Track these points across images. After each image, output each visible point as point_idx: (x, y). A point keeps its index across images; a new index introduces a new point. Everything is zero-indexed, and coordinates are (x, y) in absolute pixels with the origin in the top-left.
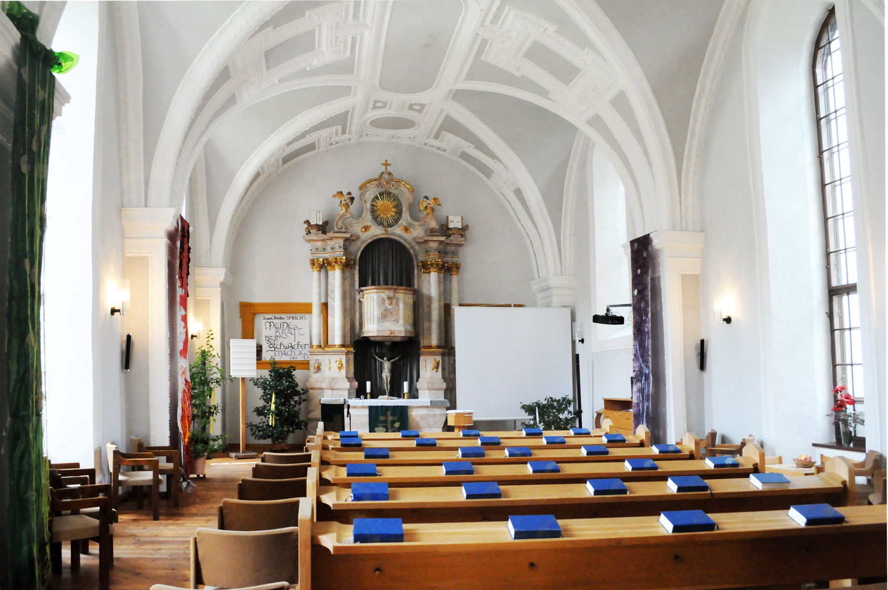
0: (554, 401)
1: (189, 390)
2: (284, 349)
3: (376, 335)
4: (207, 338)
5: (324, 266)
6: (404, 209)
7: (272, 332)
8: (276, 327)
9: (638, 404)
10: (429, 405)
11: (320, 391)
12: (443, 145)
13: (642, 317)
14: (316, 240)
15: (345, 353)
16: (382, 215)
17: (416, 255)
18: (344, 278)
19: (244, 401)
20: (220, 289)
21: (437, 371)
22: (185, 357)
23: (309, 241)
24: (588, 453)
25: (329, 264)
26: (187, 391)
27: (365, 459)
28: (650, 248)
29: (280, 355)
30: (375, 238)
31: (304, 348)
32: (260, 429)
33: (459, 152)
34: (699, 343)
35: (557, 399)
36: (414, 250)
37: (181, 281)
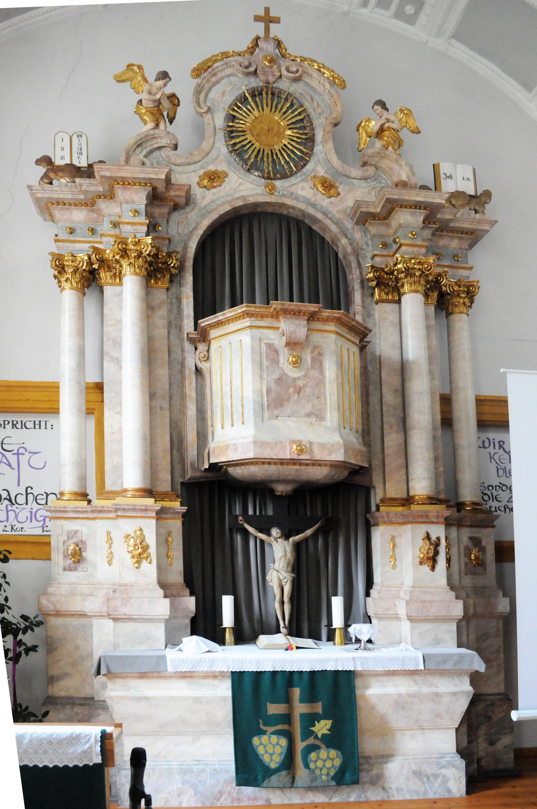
6: (319, 137)
10: (421, 667)
11: (84, 621)
15: (154, 514)
17: (356, 252)
21: (433, 568)
31: (44, 502)
36: (351, 241)
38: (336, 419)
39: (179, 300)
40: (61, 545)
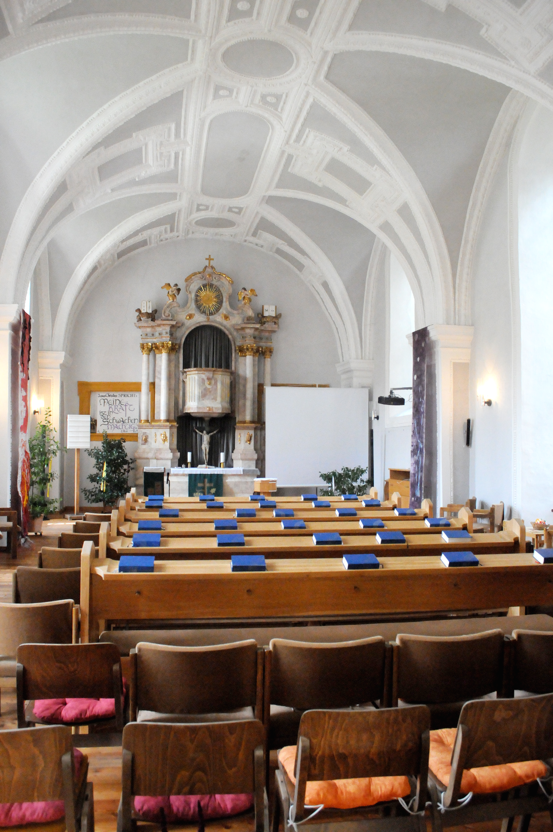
0: (349, 471)
1: (28, 460)
2: (116, 423)
3: (196, 411)
4: (46, 414)
5: (152, 349)
6: (224, 300)
7: (106, 408)
8: (110, 403)
9: (414, 474)
10: (242, 473)
11: (147, 460)
12: (260, 242)
13: (419, 399)
14: (146, 327)
16: (204, 305)
18: (169, 361)
19: (80, 469)
20: (60, 370)
22: (25, 432)
23: (139, 327)
24: (340, 515)
25: (157, 348)
26: (26, 461)
27: (160, 518)
28: (427, 340)
29: (113, 429)
30: (198, 325)
31: (134, 422)
32: (93, 494)
33: (274, 249)
34: (466, 422)
35: (352, 469)
37: (23, 366)
38: (220, 400)
39: (179, 358)
40: (141, 437)
